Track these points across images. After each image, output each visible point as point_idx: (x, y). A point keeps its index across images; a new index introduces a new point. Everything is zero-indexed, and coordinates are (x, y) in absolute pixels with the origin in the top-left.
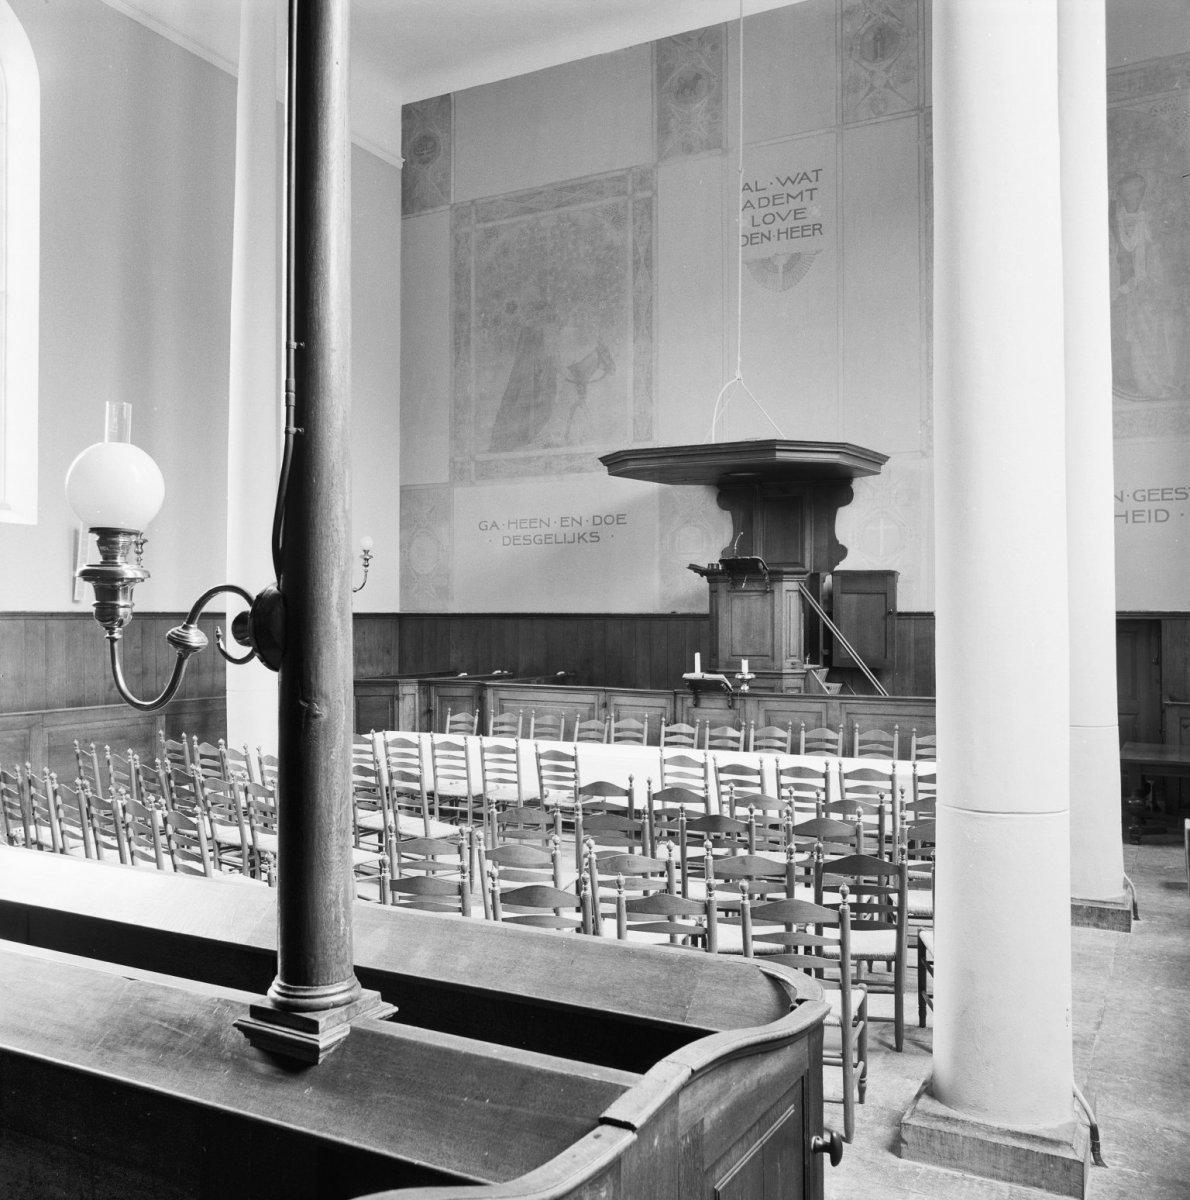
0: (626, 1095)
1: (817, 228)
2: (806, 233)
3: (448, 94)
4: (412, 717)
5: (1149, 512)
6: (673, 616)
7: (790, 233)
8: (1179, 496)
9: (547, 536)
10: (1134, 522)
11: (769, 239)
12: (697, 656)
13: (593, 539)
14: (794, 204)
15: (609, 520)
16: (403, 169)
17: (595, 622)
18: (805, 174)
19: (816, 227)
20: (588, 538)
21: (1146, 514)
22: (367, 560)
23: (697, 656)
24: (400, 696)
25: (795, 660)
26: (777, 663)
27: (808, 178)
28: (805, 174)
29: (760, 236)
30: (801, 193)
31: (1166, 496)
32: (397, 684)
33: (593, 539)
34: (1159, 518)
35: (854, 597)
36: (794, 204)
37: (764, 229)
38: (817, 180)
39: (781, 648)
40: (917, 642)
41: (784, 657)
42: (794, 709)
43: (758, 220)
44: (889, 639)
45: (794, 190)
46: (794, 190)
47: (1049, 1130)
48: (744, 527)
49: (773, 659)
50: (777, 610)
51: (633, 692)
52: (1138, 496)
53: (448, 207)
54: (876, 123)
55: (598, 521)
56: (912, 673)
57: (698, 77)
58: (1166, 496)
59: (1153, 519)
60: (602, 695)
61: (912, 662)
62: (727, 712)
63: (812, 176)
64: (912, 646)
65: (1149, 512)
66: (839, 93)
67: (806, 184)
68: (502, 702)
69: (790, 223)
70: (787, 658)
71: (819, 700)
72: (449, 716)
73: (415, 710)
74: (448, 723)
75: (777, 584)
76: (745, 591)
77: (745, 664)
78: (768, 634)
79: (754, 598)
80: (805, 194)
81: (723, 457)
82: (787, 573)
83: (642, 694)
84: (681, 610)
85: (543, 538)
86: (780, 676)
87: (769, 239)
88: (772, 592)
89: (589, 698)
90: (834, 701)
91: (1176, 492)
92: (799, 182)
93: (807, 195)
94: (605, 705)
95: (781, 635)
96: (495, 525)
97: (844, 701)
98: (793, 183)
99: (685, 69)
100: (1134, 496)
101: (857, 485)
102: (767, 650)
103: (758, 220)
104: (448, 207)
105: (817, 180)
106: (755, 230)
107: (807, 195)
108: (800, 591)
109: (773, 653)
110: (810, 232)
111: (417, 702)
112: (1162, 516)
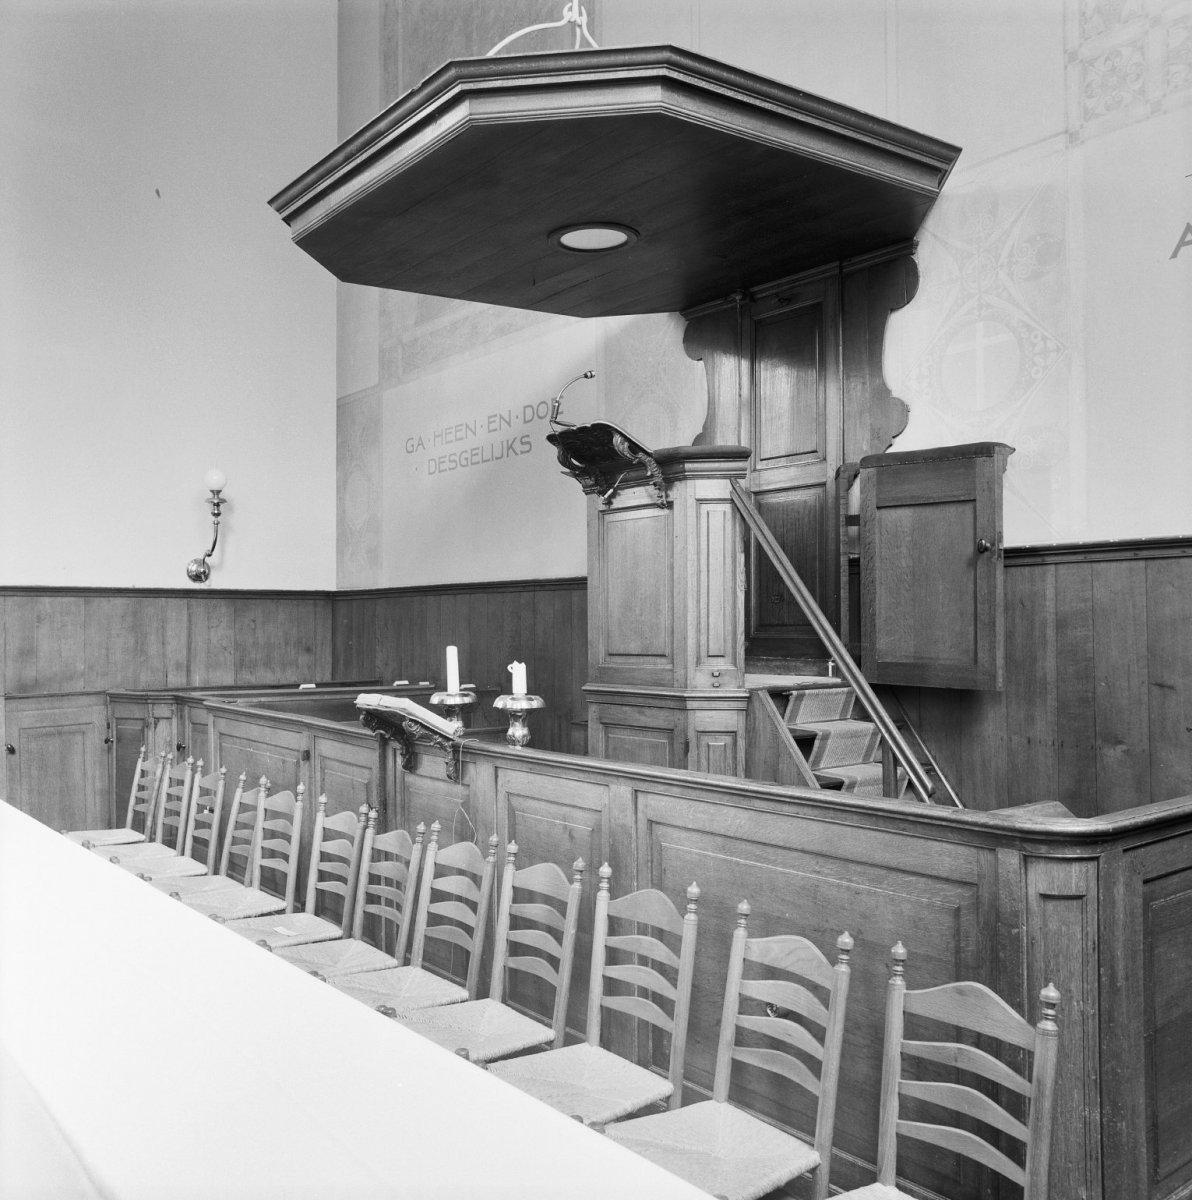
0: (1020, 1170)
9: (474, 451)
12: (452, 653)
13: (526, 439)
22: (218, 505)
23: (452, 653)
25: (722, 665)
33: (526, 439)
35: (905, 515)
40: (1061, 625)
44: (983, 618)
56: (1051, 701)
61: (1051, 676)
64: (1050, 632)
70: (698, 662)
72: (239, 791)
74: (132, 801)
77: (518, 671)
85: (468, 455)
86: (680, 703)
95: (685, 606)
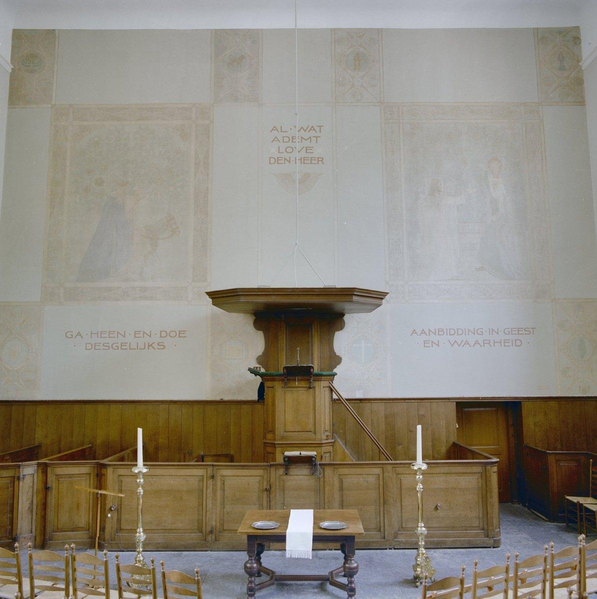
1: (320, 160)
2: (313, 162)
3: (54, 30)
4: (30, 493)
5: (447, 329)
6: (222, 402)
7: (303, 160)
8: (526, 332)
10: (505, 346)
11: (289, 162)
14: (307, 144)
15: (173, 334)
16: (11, 73)
17: (162, 406)
18: (312, 127)
19: (320, 159)
20: (155, 346)
21: (510, 341)
24: (21, 476)
26: (318, 436)
27: (314, 130)
28: (312, 127)
29: (283, 159)
30: (310, 138)
31: (520, 332)
32: (19, 466)
33: (159, 347)
34: (517, 345)
36: (307, 144)
37: (287, 156)
38: (320, 132)
39: (321, 426)
41: (323, 432)
42: (359, 473)
43: (282, 150)
45: (306, 135)
46: (306, 135)
47: (21, 529)
48: (271, 342)
49: (315, 433)
50: (317, 400)
51: (239, 466)
52: (506, 331)
53: (50, 106)
54: (355, 106)
55: (164, 334)
57: (242, 57)
58: (520, 332)
59: (448, 334)
60: (210, 469)
62: (311, 477)
63: (317, 129)
65: (447, 329)
66: (334, 84)
67: (312, 133)
68: (121, 478)
69: (303, 154)
71: (377, 466)
73: (33, 487)
75: (317, 382)
76: (298, 387)
78: (311, 416)
79: (301, 392)
80: (312, 139)
81: (314, 297)
82: (325, 376)
83: (243, 467)
84: (226, 398)
87: (289, 162)
88: (314, 387)
89: (199, 472)
90: (389, 466)
91: (525, 330)
92: (309, 132)
93: (314, 139)
94: (213, 477)
96: (79, 334)
97: (396, 466)
98: (305, 131)
99: (233, 52)
100: (504, 331)
101: (346, 318)
102: (310, 427)
103: (282, 150)
104: (50, 106)
105: (320, 132)
106: (280, 155)
107: (314, 139)
108: (330, 387)
109: (315, 429)
110: (316, 162)
111: (35, 480)
112: (518, 343)
